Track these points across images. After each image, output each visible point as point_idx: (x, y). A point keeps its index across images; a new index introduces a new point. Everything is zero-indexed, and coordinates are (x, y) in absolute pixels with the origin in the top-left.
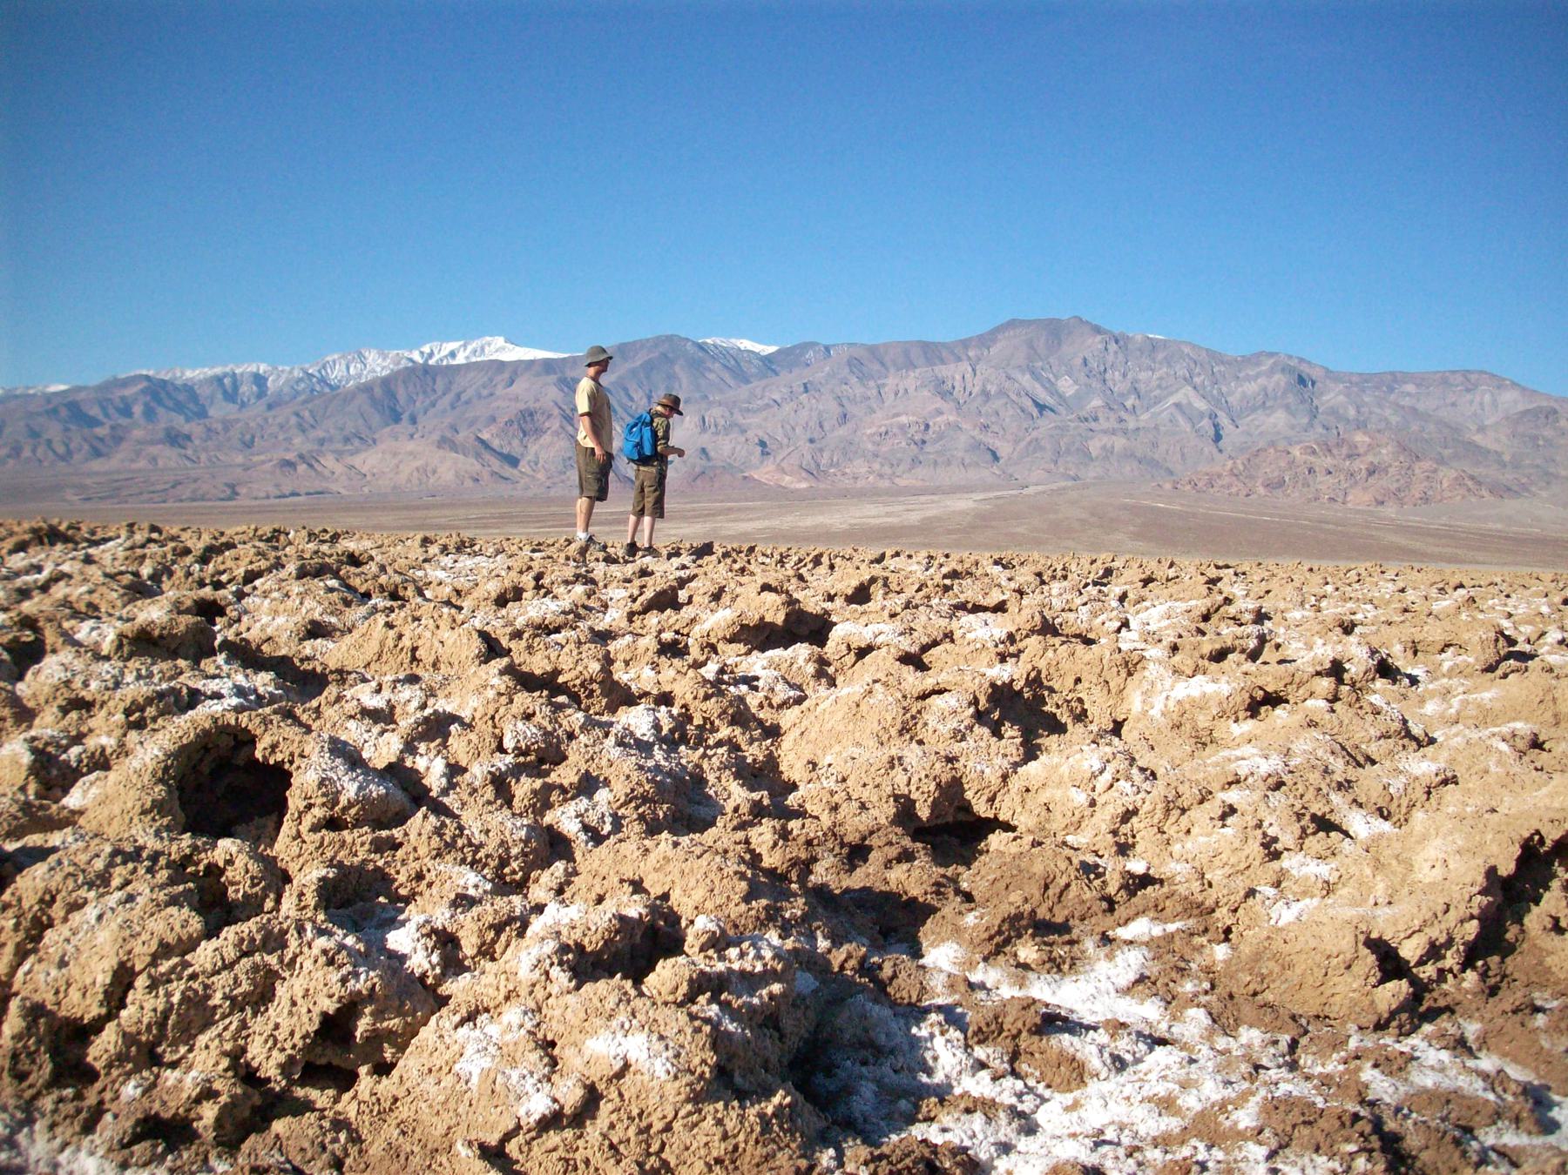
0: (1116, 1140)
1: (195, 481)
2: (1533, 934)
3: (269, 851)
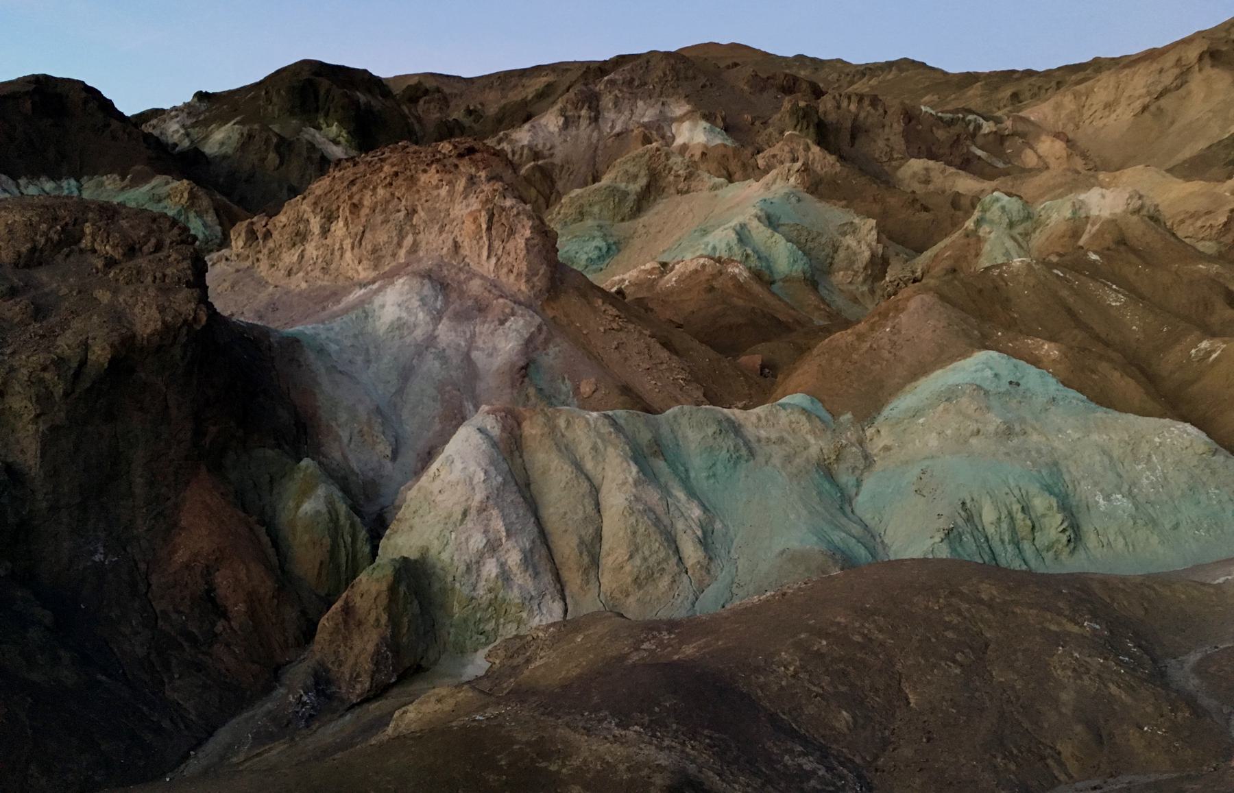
0: (490, 664)
1: (733, 583)
2: (1006, 238)
3: (431, 356)
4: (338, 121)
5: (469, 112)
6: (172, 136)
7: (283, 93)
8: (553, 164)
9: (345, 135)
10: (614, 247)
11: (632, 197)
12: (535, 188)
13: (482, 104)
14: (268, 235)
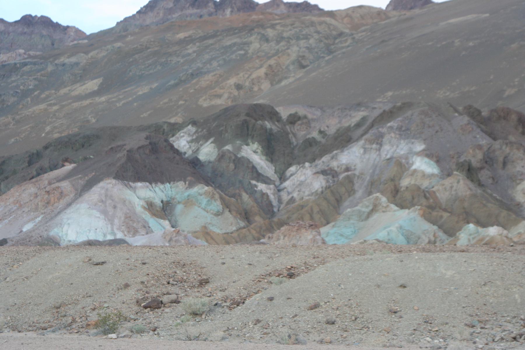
4: (257, 142)
5: (321, 132)
6: (183, 148)
7: (233, 127)
8: (355, 175)
9: (261, 149)
10: (357, 231)
11: (366, 214)
12: (345, 187)
13: (328, 127)
14: (272, 238)
